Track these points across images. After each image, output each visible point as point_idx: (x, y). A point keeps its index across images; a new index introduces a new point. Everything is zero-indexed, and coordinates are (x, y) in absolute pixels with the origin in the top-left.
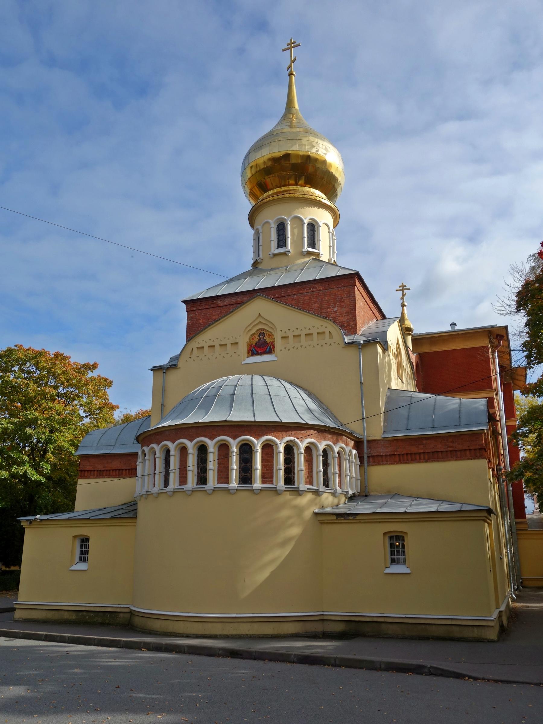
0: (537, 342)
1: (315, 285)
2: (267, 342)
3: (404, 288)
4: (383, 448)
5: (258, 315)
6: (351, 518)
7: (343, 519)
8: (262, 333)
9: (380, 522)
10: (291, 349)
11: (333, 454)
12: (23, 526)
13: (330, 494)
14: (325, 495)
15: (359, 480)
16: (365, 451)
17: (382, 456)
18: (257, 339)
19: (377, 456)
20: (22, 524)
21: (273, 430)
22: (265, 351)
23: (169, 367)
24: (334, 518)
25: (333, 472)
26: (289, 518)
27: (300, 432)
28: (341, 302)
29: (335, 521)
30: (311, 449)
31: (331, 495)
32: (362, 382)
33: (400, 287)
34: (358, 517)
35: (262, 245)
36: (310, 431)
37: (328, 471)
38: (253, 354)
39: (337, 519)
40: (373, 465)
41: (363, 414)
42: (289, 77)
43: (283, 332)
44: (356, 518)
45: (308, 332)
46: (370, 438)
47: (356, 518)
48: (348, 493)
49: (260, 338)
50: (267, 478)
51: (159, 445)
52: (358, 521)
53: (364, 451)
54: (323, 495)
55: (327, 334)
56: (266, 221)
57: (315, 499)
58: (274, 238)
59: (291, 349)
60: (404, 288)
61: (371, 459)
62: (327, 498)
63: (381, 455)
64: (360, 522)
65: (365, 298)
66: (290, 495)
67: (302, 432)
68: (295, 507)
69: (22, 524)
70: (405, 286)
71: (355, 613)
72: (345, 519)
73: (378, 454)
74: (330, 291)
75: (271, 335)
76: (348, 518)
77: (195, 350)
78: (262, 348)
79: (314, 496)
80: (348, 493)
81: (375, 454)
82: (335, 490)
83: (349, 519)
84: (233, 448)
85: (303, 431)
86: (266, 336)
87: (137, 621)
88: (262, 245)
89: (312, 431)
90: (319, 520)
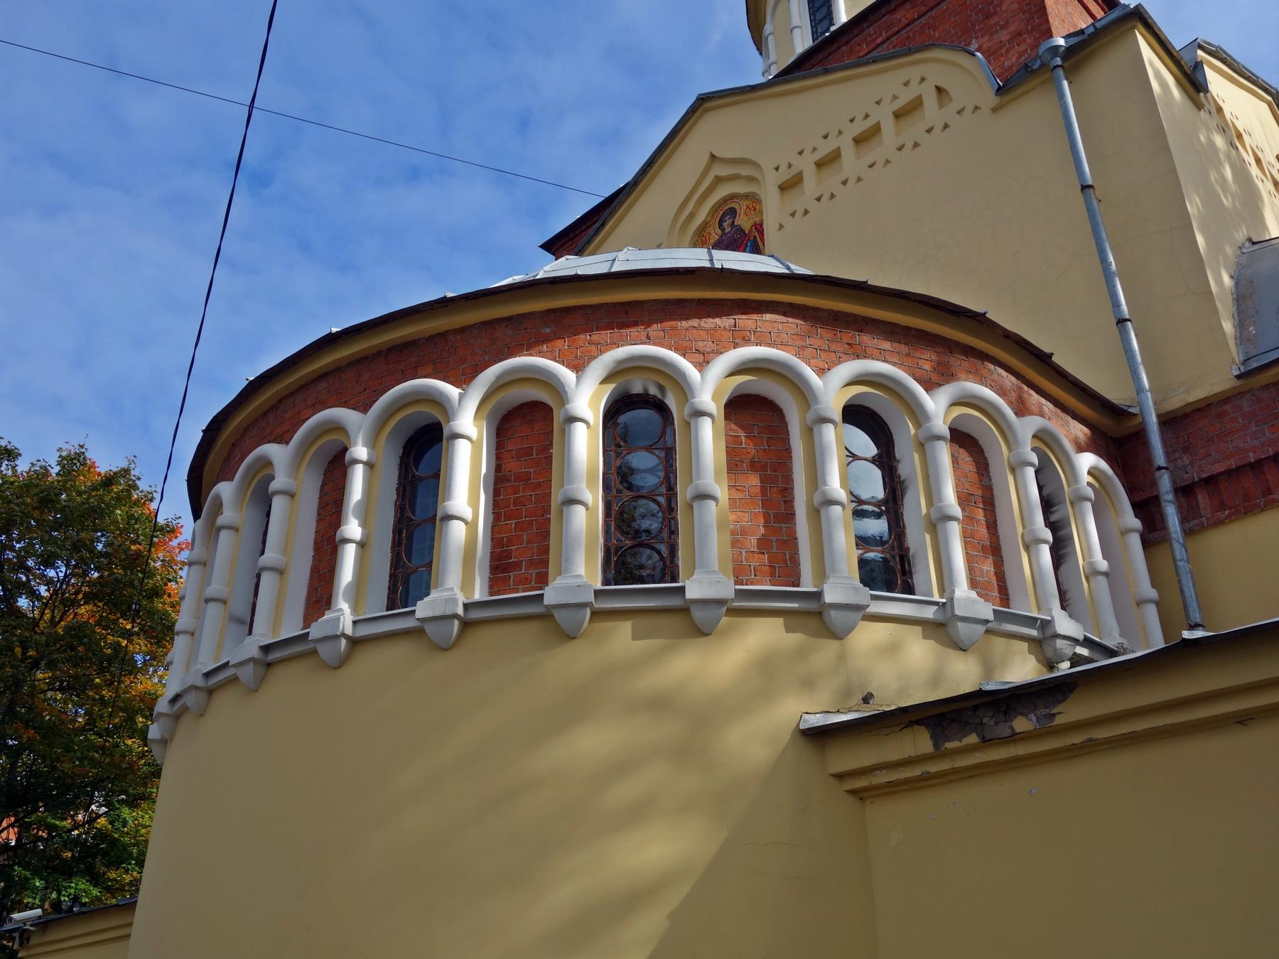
1: (894, 17)
4: (1254, 428)
5: (706, 157)
6: (1022, 724)
7: (973, 739)
9: (1243, 719)
10: (813, 206)
11: (918, 425)
13: (919, 629)
14: (867, 636)
15: (1151, 601)
16: (1160, 457)
17: (1256, 466)
19: (1229, 473)
21: (548, 330)
24: (919, 742)
25: (928, 513)
26: (621, 768)
27: (695, 322)
28: (988, 16)
29: (933, 768)
31: (925, 637)
32: (1090, 183)
34: (1070, 711)
35: (775, 63)
36: (755, 316)
37: (906, 518)
39: (939, 754)
40: (1219, 523)
41: (1116, 305)
43: (783, 168)
44: (1059, 720)
45: (860, 127)
46: (1175, 402)
47: (1059, 720)
48: (1049, 633)
49: (723, 230)
50: (517, 565)
52: (1078, 739)
53: (1149, 459)
54: (853, 633)
55: (930, 99)
57: (801, 653)
58: (800, 19)
59: (813, 206)
61: (1200, 497)
62: (892, 649)
63: (1251, 465)
64: (1091, 748)
66: (636, 636)
67: (709, 323)
68: (659, 704)
72: (986, 742)
73: (1233, 463)
74: (945, 7)
76: (1003, 730)
79: (795, 639)
80: (1049, 633)
81: (1219, 468)
82: (946, 607)
83: (1014, 738)
84: (355, 444)
85: (717, 320)
86: (740, 216)
88: (775, 63)
89: (768, 317)
90: (840, 777)
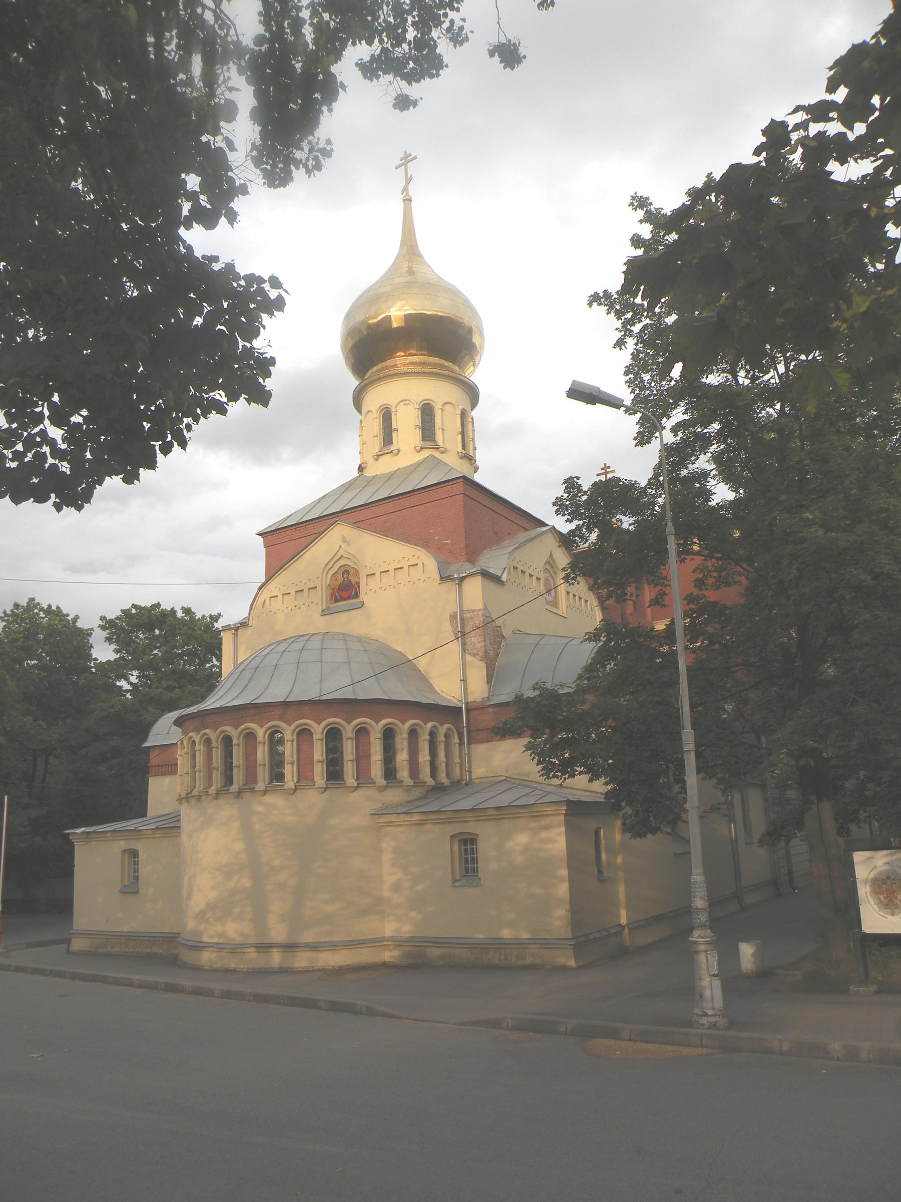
0: (47, 635)
2: (351, 583)
3: (608, 470)
8: (345, 570)
12: (71, 840)
18: (340, 579)
20: (71, 838)
22: (350, 595)
23: (239, 625)
30: (256, 736)
33: (602, 469)
38: (336, 601)
42: (403, 203)
49: (344, 578)
51: (199, 734)
55: (420, 566)
56: (368, 410)
60: (608, 470)
65: (483, 503)
69: (71, 838)
70: (609, 467)
71: (381, 942)
75: (357, 572)
77: (268, 601)
78: (347, 591)
87: (187, 956)
